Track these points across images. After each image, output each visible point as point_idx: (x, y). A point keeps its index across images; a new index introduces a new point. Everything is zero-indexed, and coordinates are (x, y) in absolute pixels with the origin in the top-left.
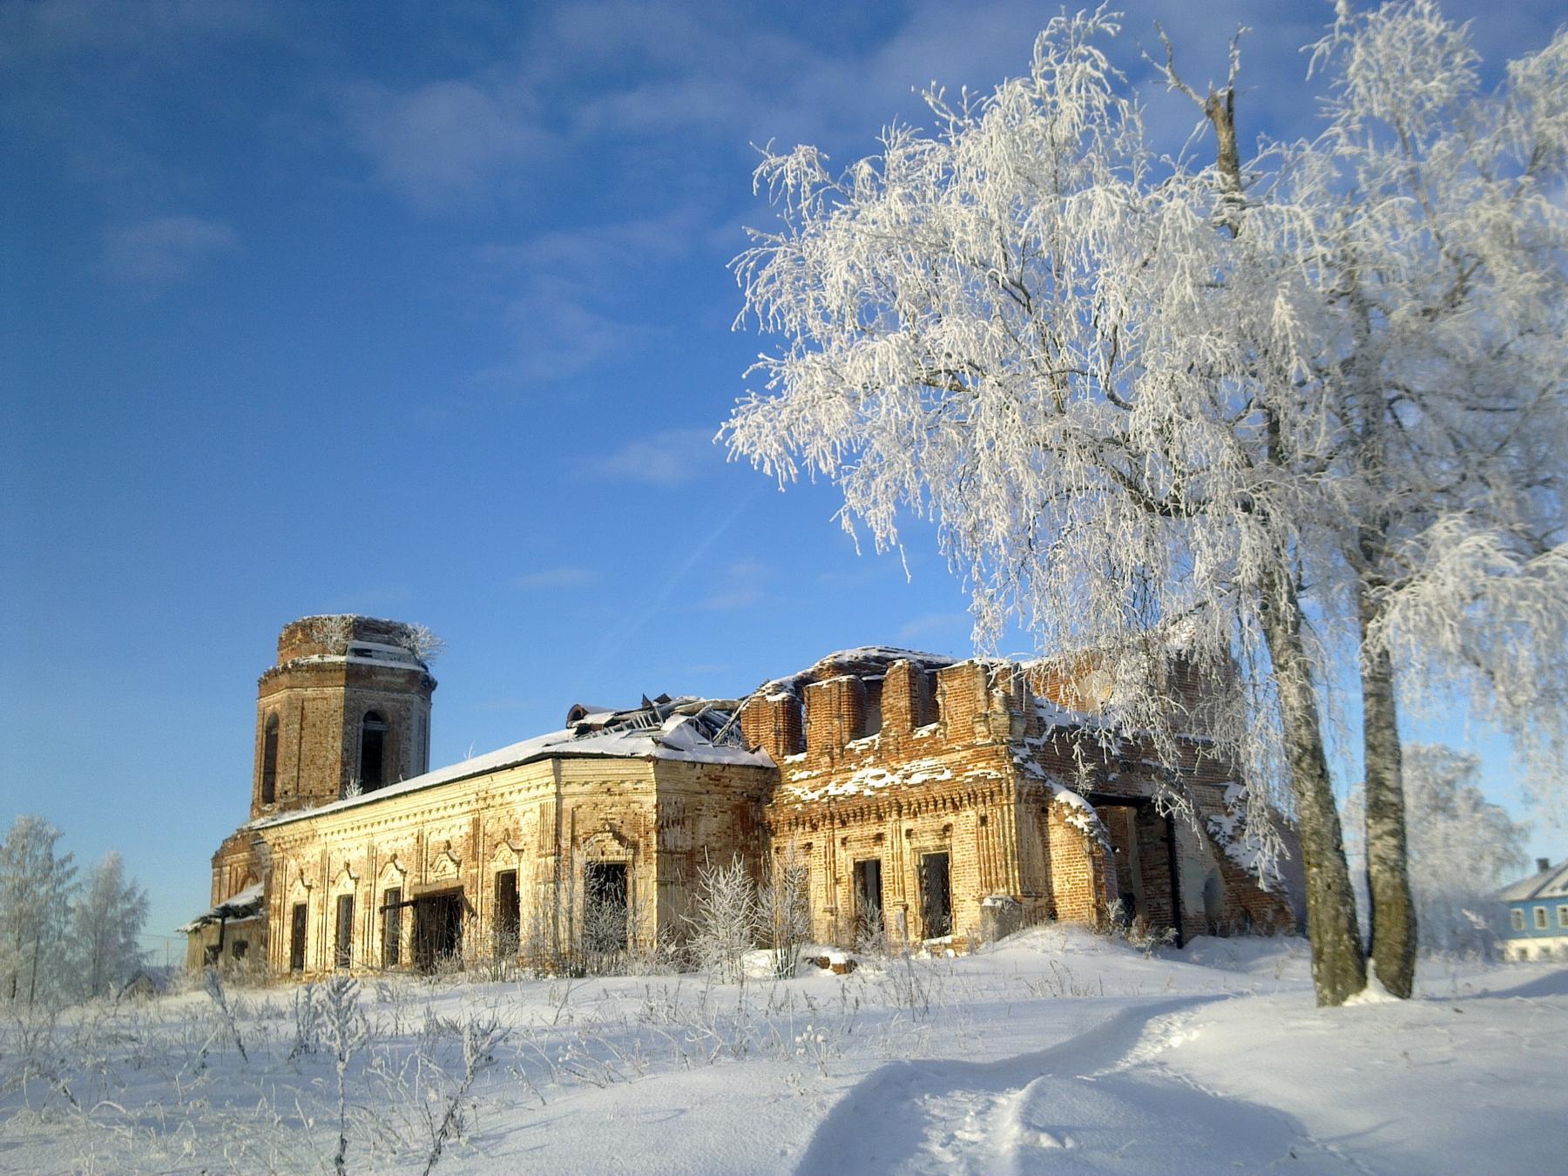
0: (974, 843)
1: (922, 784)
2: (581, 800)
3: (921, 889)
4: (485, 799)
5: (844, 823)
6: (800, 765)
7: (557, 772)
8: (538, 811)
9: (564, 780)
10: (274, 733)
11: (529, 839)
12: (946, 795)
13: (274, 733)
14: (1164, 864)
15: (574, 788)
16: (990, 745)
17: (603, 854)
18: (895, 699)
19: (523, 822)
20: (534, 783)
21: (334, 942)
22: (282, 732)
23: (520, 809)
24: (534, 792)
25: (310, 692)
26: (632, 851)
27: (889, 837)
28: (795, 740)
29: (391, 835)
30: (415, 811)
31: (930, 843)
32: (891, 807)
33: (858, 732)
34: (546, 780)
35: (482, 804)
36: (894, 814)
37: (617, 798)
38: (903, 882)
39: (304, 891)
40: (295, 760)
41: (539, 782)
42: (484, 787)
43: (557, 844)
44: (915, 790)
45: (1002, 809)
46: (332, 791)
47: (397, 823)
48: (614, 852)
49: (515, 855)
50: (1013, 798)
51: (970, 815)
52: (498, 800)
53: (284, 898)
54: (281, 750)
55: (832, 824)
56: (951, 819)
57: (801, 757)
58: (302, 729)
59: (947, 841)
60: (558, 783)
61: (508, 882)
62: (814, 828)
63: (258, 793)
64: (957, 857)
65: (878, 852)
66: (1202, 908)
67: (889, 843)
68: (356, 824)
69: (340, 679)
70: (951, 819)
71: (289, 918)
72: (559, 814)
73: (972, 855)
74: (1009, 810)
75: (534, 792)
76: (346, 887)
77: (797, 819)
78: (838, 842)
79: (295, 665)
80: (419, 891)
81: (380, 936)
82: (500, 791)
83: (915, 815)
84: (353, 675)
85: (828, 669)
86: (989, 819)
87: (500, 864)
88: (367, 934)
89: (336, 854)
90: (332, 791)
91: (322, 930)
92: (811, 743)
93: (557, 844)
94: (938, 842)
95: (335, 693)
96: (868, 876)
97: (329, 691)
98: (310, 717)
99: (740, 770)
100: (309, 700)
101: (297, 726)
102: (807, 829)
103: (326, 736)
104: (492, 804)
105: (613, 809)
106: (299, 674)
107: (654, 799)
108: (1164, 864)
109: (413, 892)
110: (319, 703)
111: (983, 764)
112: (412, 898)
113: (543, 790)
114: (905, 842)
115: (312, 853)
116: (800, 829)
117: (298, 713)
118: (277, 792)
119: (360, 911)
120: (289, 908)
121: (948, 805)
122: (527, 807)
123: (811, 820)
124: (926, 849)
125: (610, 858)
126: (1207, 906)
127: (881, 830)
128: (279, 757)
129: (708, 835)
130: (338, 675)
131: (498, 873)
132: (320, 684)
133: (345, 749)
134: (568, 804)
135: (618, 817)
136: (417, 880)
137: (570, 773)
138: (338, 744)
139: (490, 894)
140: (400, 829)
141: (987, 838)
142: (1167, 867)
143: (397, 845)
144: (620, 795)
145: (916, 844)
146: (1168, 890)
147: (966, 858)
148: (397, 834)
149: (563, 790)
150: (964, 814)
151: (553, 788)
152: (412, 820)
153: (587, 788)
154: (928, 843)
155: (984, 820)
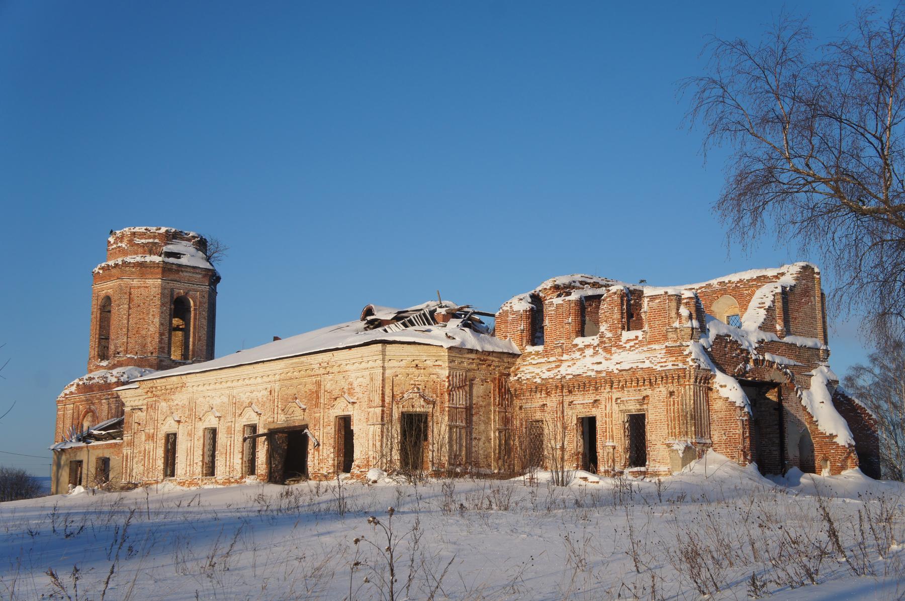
0: (664, 408)
1: (629, 369)
2: (399, 371)
3: (625, 436)
4: (325, 368)
5: (570, 392)
6: (537, 353)
7: (383, 353)
8: (368, 378)
9: (387, 358)
10: (107, 309)
11: (361, 395)
12: (646, 377)
13: (107, 309)
14: (776, 425)
15: (394, 363)
16: (679, 346)
17: (413, 406)
18: (609, 312)
19: (355, 384)
20: (365, 359)
21: (201, 459)
22: (114, 310)
23: (353, 375)
24: (364, 365)
25: (135, 282)
26: (431, 406)
27: (603, 403)
28: (535, 334)
29: (249, 389)
30: (269, 373)
31: (633, 408)
32: (606, 382)
33: (582, 333)
34: (375, 358)
35: (322, 371)
36: (608, 387)
37: (422, 371)
38: (612, 431)
39: (175, 425)
40: (125, 330)
41: (370, 358)
42: (326, 359)
43: (383, 401)
44: (624, 373)
45: (685, 387)
46: (152, 353)
47: (252, 381)
48: (419, 407)
49: (350, 406)
50: (692, 380)
51: (662, 390)
52: (336, 369)
53: (156, 428)
54: (114, 323)
55: (562, 392)
56: (649, 392)
57: (540, 348)
58: (130, 308)
59: (645, 407)
60: (383, 360)
61: (345, 425)
62: (548, 394)
63: (94, 353)
64: (650, 418)
65: (594, 412)
66: (798, 454)
67: (603, 407)
68: (220, 380)
69: (157, 273)
70: (649, 392)
71: (161, 443)
72: (383, 380)
73: (663, 416)
74: (690, 388)
75: (364, 365)
76: (211, 422)
77: (536, 388)
78: (566, 405)
79: (124, 263)
80: (272, 426)
81: (240, 456)
82: (339, 363)
83: (623, 388)
84: (167, 270)
85: (550, 289)
86: (676, 393)
87: (340, 409)
88: (228, 454)
89: (201, 399)
90: (152, 353)
91: (190, 452)
92: (547, 338)
93: (383, 401)
94: (638, 407)
95: (154, 283)
96: (589, 426)
97: (150, 282)
98: (136, 301)
99: (499, 355)
100: (134, 288)
101: (126, 306)
102: (543, 396)
103: (148, 314)
104: (331, 371)
105: (420, 378)
106: (127, 269)
107: (446, 373)
108: (776, 425)
109: (268, 427)
110: (142, 290)
111: (674, 359)
112: (266, 431)
113: (371, 364)
114: (615, 407)
115: (180, 399)
116: (538, 395)
117: (127, 296)
118: (111, 352)
119: (221, 438)
120: (161, 435)
121: (646, 383)
122: (360, 374)
123: (547, 389)
124: (629, 411)
125: (418, 410)
126: (801, 453)
127: (598, 397)
128: (112, 327)
129: (478, 397)
130: (157, 270)
131: (336, 417)
132: (142, 276)
133: (162, 324)
134: (389, 373)
135: (423, 384)
136: (271, 420)
137: (392, 353)
138: (157, 320)
139: (331, 430)
140: (255, 385)
141: (674, 404)
142: (777, 427)
143: (254, 395)
144: (424, 369)
145: (622, 407)
146: (777, 442)
147: (658, 418)
148: (253, 388)
149: (386, 365)
150: (658, 390)
151: (380, 363)
152: (266, 379)
153: (403, 363)
154: (630, 408)
155: (671, 393)
